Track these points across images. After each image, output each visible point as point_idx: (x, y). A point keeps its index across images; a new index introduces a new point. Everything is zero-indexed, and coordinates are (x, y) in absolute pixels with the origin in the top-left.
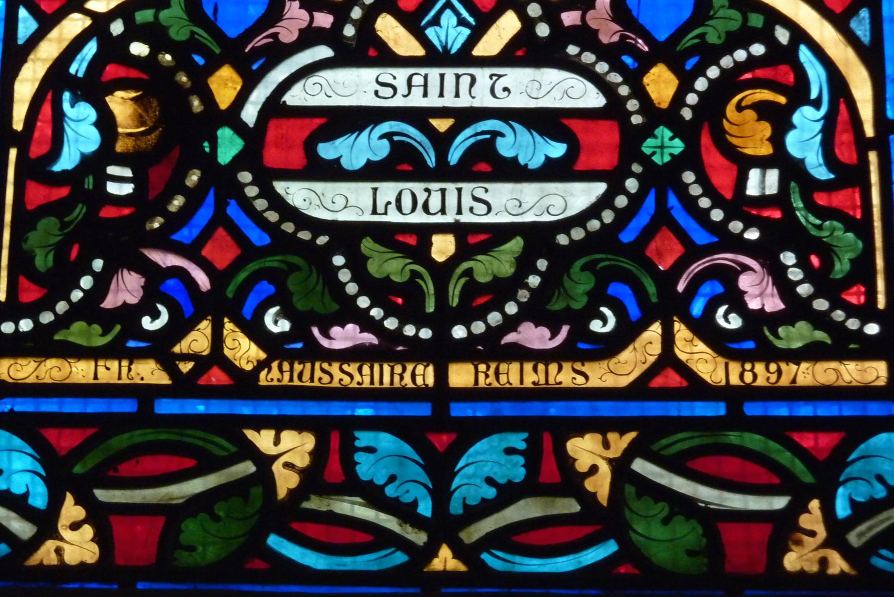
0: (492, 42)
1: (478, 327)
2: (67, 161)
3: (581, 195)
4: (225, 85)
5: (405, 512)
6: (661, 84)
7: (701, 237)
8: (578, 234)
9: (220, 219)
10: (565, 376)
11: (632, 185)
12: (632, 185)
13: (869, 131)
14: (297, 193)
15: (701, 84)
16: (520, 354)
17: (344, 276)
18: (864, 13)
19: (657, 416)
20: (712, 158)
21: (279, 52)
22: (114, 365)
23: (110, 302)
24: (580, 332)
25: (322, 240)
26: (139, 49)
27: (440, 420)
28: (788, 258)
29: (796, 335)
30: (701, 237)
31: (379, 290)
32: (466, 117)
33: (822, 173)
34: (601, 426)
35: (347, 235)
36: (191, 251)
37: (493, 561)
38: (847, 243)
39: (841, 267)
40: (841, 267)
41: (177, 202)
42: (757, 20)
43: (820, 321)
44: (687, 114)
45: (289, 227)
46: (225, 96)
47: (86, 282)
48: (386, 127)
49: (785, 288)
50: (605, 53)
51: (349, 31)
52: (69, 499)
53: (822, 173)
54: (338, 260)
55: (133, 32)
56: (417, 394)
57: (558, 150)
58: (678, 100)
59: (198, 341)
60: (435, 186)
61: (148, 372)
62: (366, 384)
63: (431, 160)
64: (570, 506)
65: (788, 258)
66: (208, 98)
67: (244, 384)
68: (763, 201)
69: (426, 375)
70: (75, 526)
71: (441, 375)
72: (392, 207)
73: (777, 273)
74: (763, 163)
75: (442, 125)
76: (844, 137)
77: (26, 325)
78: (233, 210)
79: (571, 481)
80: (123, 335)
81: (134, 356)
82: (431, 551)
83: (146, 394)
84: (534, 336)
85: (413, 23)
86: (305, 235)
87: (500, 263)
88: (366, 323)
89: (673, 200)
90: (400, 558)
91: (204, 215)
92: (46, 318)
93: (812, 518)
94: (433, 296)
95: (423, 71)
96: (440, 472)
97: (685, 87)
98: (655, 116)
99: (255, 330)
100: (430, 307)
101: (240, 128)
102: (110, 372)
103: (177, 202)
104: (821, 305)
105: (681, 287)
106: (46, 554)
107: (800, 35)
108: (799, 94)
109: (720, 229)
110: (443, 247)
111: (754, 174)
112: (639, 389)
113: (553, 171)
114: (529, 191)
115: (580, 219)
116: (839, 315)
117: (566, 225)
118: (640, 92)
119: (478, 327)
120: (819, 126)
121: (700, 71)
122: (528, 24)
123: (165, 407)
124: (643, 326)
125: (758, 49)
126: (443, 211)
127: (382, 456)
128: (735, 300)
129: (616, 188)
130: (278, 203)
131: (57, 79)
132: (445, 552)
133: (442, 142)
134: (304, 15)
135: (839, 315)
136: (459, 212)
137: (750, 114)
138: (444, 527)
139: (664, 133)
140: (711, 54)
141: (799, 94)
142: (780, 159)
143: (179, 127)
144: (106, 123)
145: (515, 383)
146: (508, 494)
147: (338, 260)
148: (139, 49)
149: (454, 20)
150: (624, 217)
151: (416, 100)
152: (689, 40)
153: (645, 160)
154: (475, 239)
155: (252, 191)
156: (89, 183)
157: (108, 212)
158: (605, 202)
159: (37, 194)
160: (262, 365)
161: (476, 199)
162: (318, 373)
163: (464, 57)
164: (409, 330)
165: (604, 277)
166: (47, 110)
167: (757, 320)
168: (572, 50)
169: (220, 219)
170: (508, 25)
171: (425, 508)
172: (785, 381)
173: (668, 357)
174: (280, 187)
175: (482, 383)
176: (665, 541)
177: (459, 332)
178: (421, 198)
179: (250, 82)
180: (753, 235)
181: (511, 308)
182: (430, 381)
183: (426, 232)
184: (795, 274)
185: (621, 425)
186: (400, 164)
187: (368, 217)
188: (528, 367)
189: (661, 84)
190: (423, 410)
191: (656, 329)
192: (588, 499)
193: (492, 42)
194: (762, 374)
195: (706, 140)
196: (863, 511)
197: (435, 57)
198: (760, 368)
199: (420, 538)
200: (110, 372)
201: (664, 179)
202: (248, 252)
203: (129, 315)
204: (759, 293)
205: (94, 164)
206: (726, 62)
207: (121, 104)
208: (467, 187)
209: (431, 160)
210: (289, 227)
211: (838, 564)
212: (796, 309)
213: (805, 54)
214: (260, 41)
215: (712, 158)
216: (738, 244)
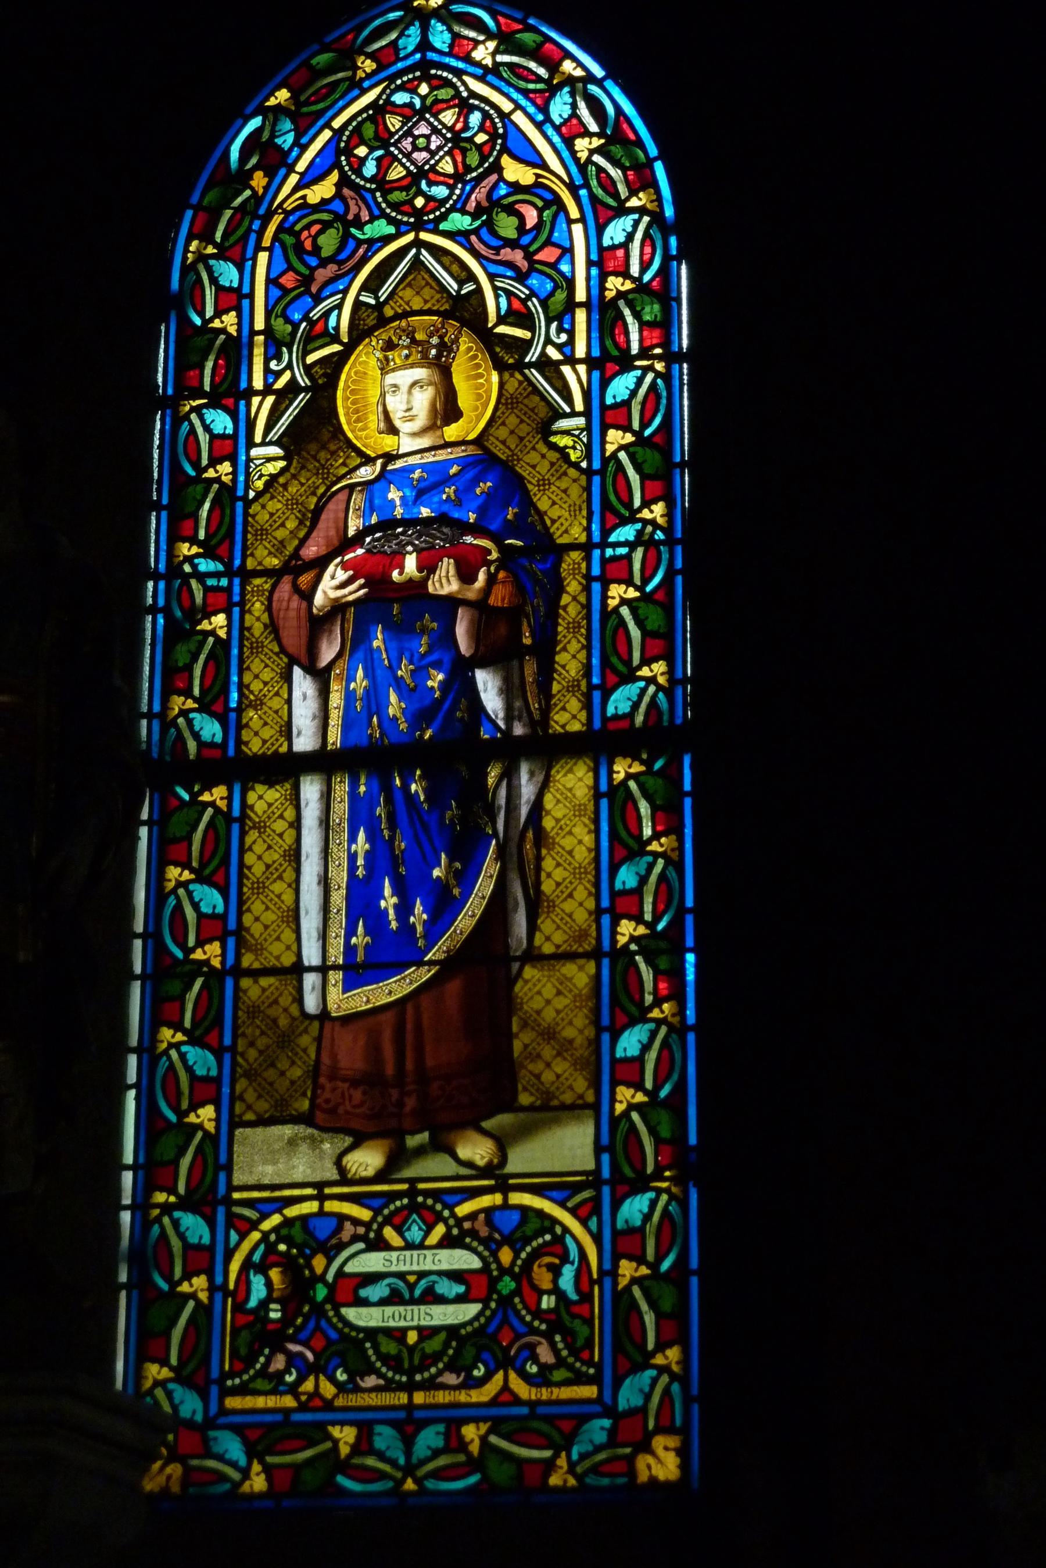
0: (434, 1238)
1: (426, 1375)
2: (253, 1303)
3: (472, 1310)
4: (319, 1263)
5: (393, 1463)
6: (506, 1255)
7: (522, 1329)
8: (469, 1329)
9: (318, 1328)
10: (462, 1397)
11: (493, 1305)
12: (493, 1305)
13: (595, 1276)
14: (351, 1314)
15: (523, 1255)
16: (444, 1387)
17: (370, 1352)
18: (595, 1219)
19: (502, 1416)
20: (526, 1290)
21: (341, 1246)
22: (273, 1398)
23: (271, 1369)
24: (469, 1376)
25: (361, 1335)
26: (282, 1247)
27: (410, 1420)
28: (558, 1338)
29: (558, 1375)
30: (522, 1329)
31: (385, 1359)
32: (422, 1275)
33: (574, 1297)
34: (476, 1420)
35: (372, 1333)
36: (305, 1344)
37: (430, 1484)
38: (583, 1331)
39: (580, 1343)
40: (580, 1343)
41: (299, 1320)
42: (547, 1223)
43: (570, 1368)
44: (517, 1269)
45: (346, 1330)
46: (319, 1271)
47: (262, 1359)
48: (387, 1281)
49: (556, 1352)
50: (482, 1241)
51: (372, 1235)
52: (255, 1462)
53: (574, 1297)
54: (368, 1345)
55: (280, 1240)
56: (401, 1407)
57: (461, 1289)
58: (513, 1263)
59: (309, 1385)
60: (409, 1308)
61: (289, 1401)
62: (379, 1403)
63: (407, 1296)
64: (462, 1458)
65: (558, 1338)
66: (312, 1270)
67: (328, 1405)
68: (549, 1311)
69: (403, 1398)
70: (258, 1474)
71: (410, 1398)
72: (391, 1320)
73: (553, 1345)
74: (549, 1293)
75: (412, 1279)
76: (585, 1279)
77: (237, 1381)
78: (323, 1323)
79: (462, 1446)
80: (276, 1384)
81: (282, 1394)
82: (403, 1481)
83: (286, 1412)
84: (451, 1379)
85: (399, 1230)
86: (354, 1334)
87: (434, 1345)
88: (380, 1375)
89: (510, 1313)
90: (391, 1484)
91: (311, 1325)
92: (245, 1377)
93: (562, 1462)
94: (407, 1360)
95: (404, 1253)
96: (408, 1443)
97: (517, 1256)
98: (503, 1271)
99: (332, 1380)
100: (406, 1365)
101: (326, 1283)
102: (271, 1402)
103: (299, 1320)
104: (571, 1360)
105: (512, 1353)
106: (246, 1487)
107: (566, 1230)
108: (565, 1259)
109: (529, 1325)
110: (412, 1337)
111: (545, 1298)
112: (494, 1402)
113: (460, 1299)
114: (450, 1308)
115: (470, 1322)
116: (578, 1365)
117: (464, 1325)
118: (498, 1261)
119: (426, 1375)
120: (573, 1273)
121: (523, 1249)
122: (449, 1228)
123: (297, 1417)
124: (496, 1372)
125: (548, 1237)
126: (412, 1320)
127: (385, 1438)
128: (535, 1360)
129: (486, 1306)
130: (342, 1319)
131: (247, 1265)
132: (409, 1481)
133: (411, 1287)
134: (352, 1228)
135: (578, 1365)
136: (419, 1320)
137: (544, 1269)
138: (409, 1470)
139: (507, 1279)
140: (528, 1241)
141: (565, 1259)
142: (556, 1291)
143: (299, 1286)
144: (269, 1284)
145: (441, 1401)
146: (436, 1453)
147: (368, 1345)
148: (282, 1247)
149: (417, 1228)
150: (489, 1320)
151: (403, 1268)
152: (518, 1234)
153: (499, 1293)
154: (426, 1333)
155: (331, 1313)
156: (262, 1313)
157: (271, 1327)
158: (481, 1313)
159: (242, 1319)
160: (336, 1396)
161: (426, 1314)
162: (359, 1399)
163: (421, 1246)
164: (397, 1377)
165: (480, 1349)
166: (243, 1277)
167: (544, 1368)
168: (468, 1240)
169: (318, 1328)
170: (440, 1230)
171: (402, 1461)
172: (554, 1397)
173: (506, 1387)
174: (344, 1311)
175: (427, 1401)
176: (502, 1474)
177: (418, 1377)
178: (403, 1314)
179: (330, 1261)
180: (543, 1327)
181: (441, 1365)
182: (406, 1401)
183: (404, 1331)
184: (560, 1346)
185: (485, 1420)
186: (394, 1298)
187: (381, 1324)
188: (447, 1392)
189: (506, 1255)
190: (402, 1415)
191: (501, 1373)
192: (469, 1454)
193: (434, 1238)
194: (545, 1394)
195: (525, 1283)
196: (583, 1457)
197: (409, 1246)
198: (544, 1390)
199: (399, 1475)
200: (271, 1402)
201: (505, 1302)
202: (330, 1342)
203: (280, 1375)
204: (545, 1354)
205: (264, 1304)
206: (534, 1244)
207: (275, 1274)
208: (422, 1307)
209: (407, 1296)
210: (346, 1330)
211: (572, 1482)
212: (561, 1363)
213: (568, 1240)
214: (334, 1241)
215: (526, 1290)
216: (536, 1332)
